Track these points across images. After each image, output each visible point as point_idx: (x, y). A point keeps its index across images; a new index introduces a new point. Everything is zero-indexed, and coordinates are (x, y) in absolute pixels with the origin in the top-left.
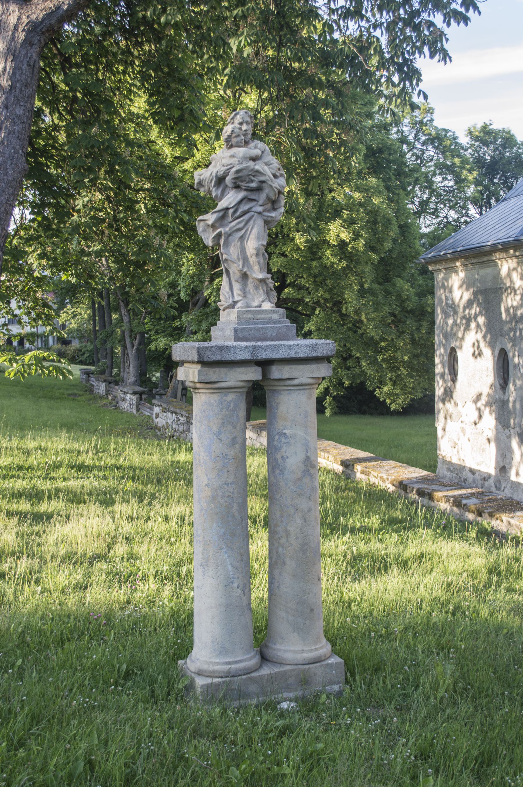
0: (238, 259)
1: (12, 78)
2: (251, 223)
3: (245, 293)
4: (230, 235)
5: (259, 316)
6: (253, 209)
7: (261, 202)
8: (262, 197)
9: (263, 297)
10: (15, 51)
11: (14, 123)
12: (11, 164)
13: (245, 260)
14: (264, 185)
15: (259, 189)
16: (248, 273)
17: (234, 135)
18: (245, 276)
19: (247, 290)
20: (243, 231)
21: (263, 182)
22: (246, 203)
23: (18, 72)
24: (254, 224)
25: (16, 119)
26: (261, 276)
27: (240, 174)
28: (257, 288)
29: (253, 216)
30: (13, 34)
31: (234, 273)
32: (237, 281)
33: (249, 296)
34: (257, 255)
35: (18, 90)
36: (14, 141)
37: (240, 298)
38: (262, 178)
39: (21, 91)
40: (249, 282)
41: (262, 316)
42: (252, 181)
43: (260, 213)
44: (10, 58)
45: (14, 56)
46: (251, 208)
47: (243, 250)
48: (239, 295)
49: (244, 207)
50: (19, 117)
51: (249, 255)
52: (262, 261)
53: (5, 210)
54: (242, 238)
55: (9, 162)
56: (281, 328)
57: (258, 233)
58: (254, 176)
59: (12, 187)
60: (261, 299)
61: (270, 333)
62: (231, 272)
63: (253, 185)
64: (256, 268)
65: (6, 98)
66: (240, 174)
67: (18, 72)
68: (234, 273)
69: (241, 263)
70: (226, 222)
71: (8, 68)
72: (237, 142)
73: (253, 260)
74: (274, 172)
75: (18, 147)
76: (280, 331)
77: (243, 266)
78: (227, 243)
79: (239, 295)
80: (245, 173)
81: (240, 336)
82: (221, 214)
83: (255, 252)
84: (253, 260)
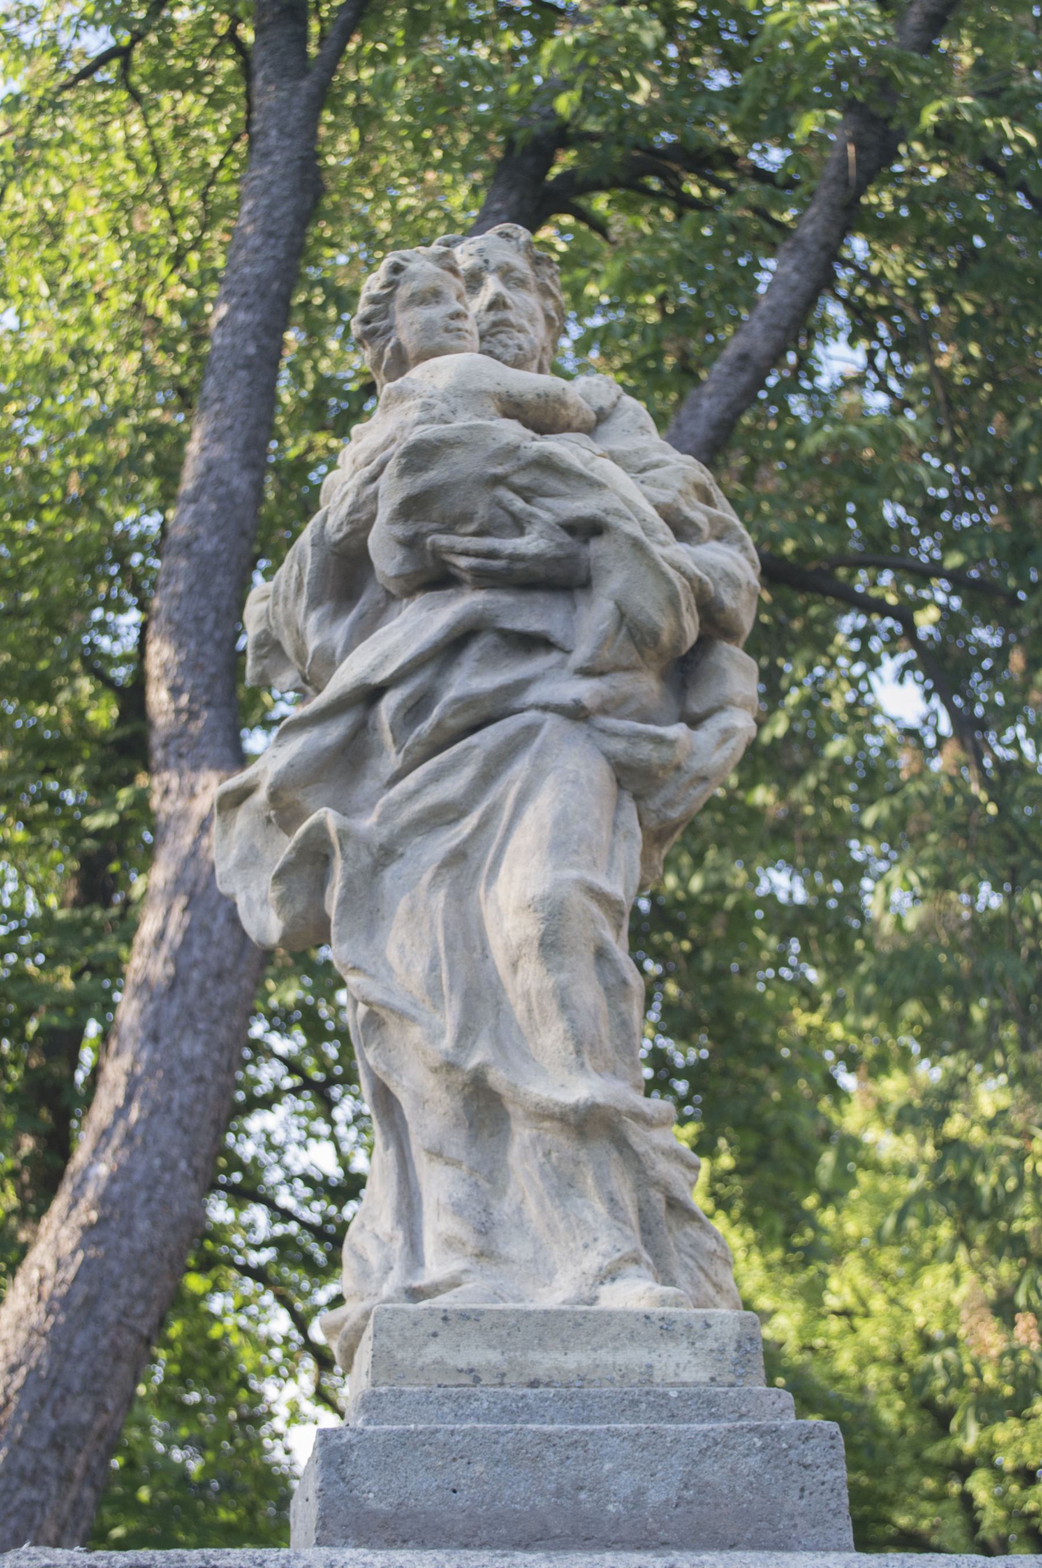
0: (434, 991)
1: (175, 958)
2: (520, 768)
3: (484, 1229)
4: (387, 854)
5: (547, 1361)
6: (536, 694)
7: (581, 654)
8: (589, 625)
9: (607, 1243)
10: (195, 884)
11: (170, 1081)
12: (149, 1200)
13: (480, 1000)
14: (597, 547)
15: (561, 580)
16: (497, 1078)
17: (403, 292)
18: (483, 1107)
19: (504, 1208)
20: (468, 824)
21: (590, 529)
22: (486, 662)
23: (198, 941)
24: (537, 775)
25: (179, 1071)
26: (580, 1089)
27: (434, 475)
28: (563, 1185)
29: (531, 731)
30: (196, 841)
31: (421, 1101)
32: (436, 1153)
33: (516, 1249)
34: (551, 945)
35: (193, 989)
36: (166, 1132)
37: (455, 1265)
38: (583, 506)
39: (202, 991)
40: (515, 1153)
41: (574, 1360)
42: (518, 525)
43: (576, 713)
44: (181, 901)
45: (191, 896)
46: (521, 686)
47: (466, 937)
48: (450, 1243)
49: (470, 679)
50: (188, 1065)
51: (500, 958)
52: (589, 994)
53: (113, 1344)
54: (458, 857)
55: (142, 1196)
56: (712, 1447)
57: (562, 821)
58: (527, 494)
59: (143, 1273)
60: (592, 1261)
61: (626, 1483)
62: (404, 1098)
63: (530, 544)
64: (551, 1039)
65: (157, 1014)
66: (434, 475)
67: (198, 941)
68: (421, 1101)
69: (449, 1019)
70: (370, 784)
71: (171, 931)
72: (428, 328)
73: (526, 982)
74: (665, 497)
75: (175, 1152)
76: (712, 1472)
77: (466, 1034)
78: (367, 905)
79: (450, 1243)
80: (462, 464)
81: (373, 1496)
82: (335, 732)
83: (530, 928)
84: (526, 982)
